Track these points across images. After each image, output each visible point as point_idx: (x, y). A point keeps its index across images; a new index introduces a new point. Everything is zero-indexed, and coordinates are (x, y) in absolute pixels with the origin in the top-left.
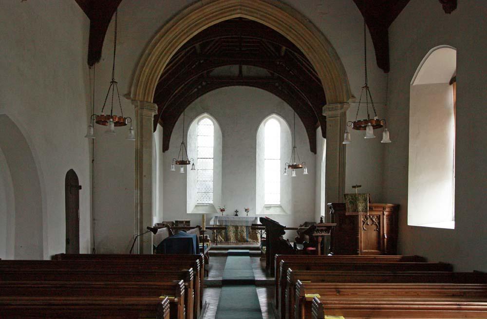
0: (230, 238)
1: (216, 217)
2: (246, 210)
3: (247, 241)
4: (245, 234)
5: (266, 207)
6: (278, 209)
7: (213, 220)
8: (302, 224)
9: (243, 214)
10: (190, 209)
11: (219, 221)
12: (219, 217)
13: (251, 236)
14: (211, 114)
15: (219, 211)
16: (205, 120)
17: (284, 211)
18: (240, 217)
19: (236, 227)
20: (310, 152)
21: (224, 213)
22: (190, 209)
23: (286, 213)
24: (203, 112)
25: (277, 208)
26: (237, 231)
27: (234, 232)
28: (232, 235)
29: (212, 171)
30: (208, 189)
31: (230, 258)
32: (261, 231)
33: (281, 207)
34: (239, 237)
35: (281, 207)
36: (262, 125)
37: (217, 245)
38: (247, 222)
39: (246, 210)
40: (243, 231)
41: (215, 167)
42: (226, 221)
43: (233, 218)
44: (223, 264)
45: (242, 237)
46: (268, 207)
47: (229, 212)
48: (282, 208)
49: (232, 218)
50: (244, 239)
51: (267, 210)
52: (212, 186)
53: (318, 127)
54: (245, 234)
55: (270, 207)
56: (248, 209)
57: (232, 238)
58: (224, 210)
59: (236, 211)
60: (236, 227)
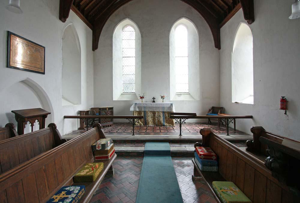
0: (149, 123)
1: (136, 104)
2: (162, 97)
3: (164, 126)
4: (162, 119)
5: (177, 95)
6: (188, 96)
7: (133, 106)
8: (210, 109)
9: (159, 101)
10: (117, 95)
11: (138, 107)
12: (139, 104)
13: (167, 120)
14: (132, 19)
15: (139, 98)
16: (128, 27)
17: (192, 97)
18: (157, 104)
19: (154, 113)
20: (215, 48)
21: (143, 100)
22: (117, 95)
23: (194, 99)
24: (124, 18)
25: (187, 95)
26: (154, 116)
27: (152, 117)
28: (150, 119)
29: (135, 67)
30: (131, 81)
31: (147, 160)
32: (180, 120)
33: (189, 94)
34: (156, 121)
35: (189, 94)
36: (173, 29)
37: (133, 135)
38: (163, 108)
39: (162, 97)
40: (160, 116)
41: (136, 63)
42: (144, 107)
43: (151, 104)
44: (140, 166)
45: (159, 121)
46: (179, 94)
47: (148, 99)
48: (191, 95)
49: (150, 103)
50: (161, 123)
51: (178, 96)
52: (134, 79)
53: (240, 9)
54: (162, 119)
55: (181, 94)
56: (164, 96)
57: (150, 123)
58: (143, 98)
59: (154, 98)
60: (154, 113)
